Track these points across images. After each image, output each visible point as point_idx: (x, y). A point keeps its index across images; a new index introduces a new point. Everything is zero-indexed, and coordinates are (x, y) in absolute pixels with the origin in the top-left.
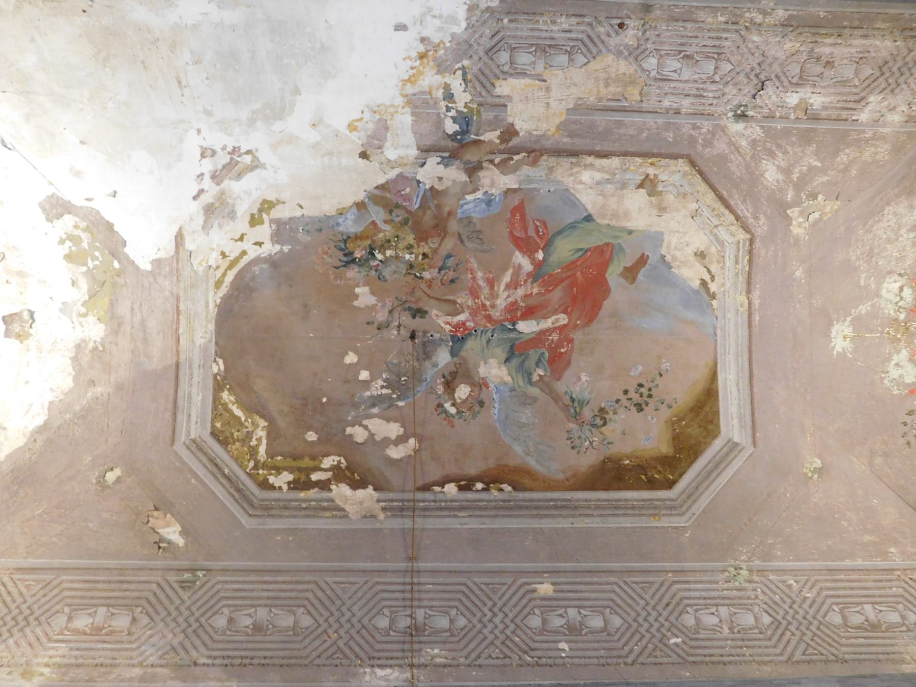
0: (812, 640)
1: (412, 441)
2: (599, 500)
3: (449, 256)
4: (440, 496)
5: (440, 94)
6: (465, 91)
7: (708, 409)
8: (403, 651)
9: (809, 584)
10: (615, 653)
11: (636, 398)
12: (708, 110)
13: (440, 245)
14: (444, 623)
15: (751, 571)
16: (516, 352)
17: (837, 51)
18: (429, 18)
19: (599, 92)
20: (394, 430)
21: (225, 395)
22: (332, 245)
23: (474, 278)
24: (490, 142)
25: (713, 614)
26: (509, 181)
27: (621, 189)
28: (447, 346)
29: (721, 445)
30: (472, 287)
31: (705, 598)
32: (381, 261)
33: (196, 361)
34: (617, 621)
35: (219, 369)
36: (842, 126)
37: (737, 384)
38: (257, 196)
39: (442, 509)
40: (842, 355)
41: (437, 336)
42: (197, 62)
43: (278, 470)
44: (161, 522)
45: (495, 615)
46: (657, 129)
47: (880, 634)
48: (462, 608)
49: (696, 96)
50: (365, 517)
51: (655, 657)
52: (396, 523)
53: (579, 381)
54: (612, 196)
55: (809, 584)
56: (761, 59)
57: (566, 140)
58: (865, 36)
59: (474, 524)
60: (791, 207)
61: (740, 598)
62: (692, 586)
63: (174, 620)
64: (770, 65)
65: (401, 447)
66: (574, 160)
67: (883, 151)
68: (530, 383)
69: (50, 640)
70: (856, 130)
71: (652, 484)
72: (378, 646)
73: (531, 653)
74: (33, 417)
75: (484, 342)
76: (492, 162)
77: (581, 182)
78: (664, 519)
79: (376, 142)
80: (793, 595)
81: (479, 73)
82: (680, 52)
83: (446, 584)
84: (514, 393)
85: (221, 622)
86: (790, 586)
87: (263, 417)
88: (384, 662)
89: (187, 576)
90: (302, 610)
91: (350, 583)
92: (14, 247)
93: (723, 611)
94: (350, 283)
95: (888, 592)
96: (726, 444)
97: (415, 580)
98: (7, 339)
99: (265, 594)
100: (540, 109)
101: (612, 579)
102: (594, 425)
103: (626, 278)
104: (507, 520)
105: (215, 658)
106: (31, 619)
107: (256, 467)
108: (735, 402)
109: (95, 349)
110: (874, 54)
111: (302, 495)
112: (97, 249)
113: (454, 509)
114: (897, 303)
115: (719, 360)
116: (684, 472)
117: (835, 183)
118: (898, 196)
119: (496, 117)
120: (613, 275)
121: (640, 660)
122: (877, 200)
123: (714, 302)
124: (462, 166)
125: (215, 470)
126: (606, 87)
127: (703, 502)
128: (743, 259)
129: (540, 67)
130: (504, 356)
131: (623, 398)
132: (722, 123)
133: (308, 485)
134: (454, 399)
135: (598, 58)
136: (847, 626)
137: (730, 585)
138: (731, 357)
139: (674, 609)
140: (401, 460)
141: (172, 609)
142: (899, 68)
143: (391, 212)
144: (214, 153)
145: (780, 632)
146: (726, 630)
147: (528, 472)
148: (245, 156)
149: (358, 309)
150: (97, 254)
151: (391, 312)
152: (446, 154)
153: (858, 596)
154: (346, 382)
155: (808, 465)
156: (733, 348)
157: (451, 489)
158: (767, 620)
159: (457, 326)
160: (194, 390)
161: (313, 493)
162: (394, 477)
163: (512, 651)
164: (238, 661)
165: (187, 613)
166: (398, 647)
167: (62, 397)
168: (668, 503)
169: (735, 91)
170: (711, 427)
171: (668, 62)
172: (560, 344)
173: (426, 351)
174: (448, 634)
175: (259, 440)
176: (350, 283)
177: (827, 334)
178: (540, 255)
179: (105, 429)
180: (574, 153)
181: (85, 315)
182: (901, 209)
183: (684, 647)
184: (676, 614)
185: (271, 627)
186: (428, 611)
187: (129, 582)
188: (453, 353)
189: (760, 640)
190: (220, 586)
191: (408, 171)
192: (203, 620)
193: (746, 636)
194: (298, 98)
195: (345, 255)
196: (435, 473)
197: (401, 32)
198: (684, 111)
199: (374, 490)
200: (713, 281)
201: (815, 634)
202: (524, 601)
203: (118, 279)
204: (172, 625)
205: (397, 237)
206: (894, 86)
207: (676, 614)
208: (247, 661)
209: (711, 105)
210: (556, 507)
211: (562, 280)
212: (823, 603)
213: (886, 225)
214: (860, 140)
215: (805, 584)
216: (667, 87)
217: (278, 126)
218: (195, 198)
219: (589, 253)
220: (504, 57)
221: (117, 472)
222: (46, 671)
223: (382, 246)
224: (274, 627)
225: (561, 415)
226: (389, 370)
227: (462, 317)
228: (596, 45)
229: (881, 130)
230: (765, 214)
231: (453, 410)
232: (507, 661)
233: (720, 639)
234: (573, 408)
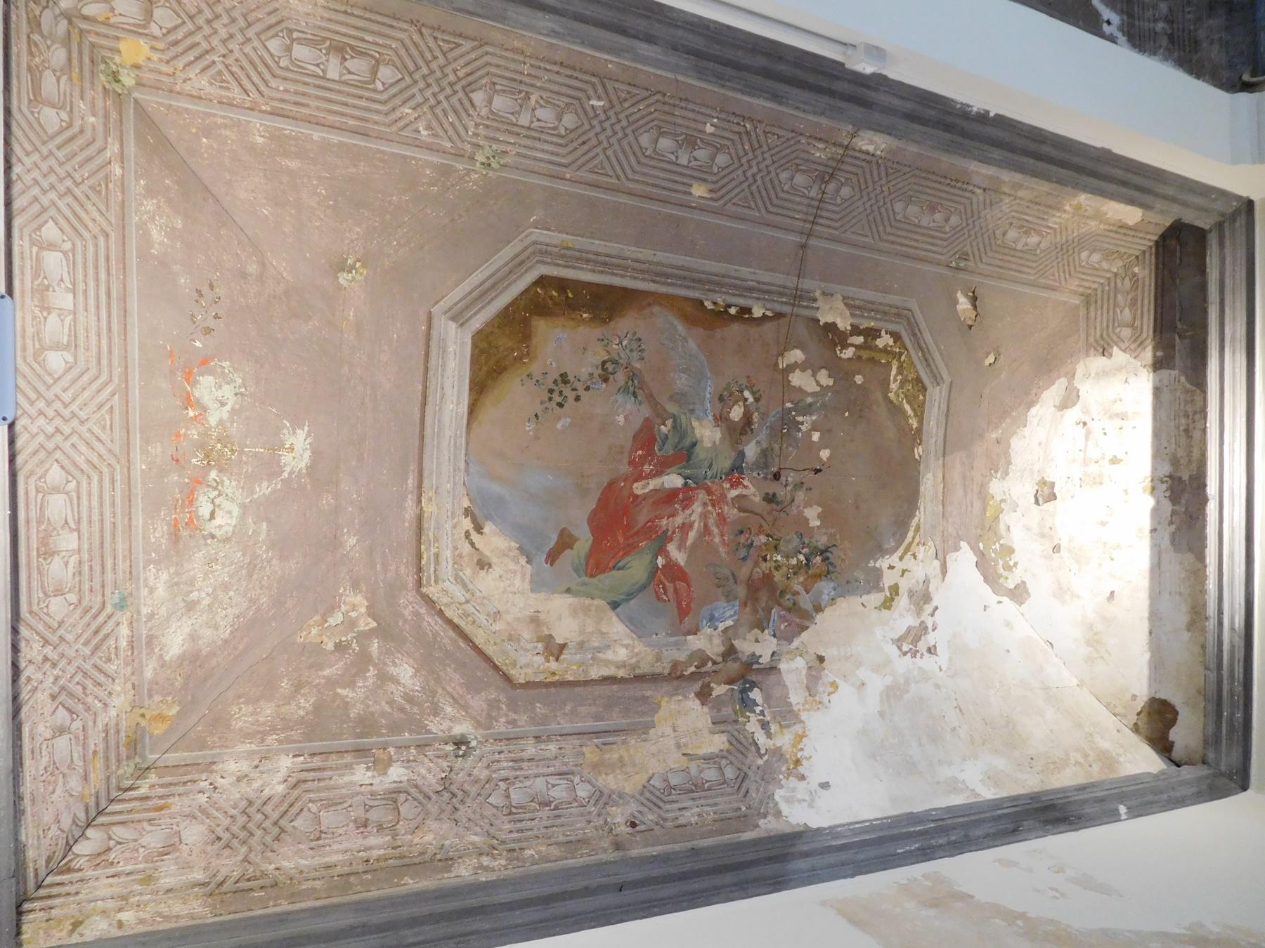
0: (435, 58)
2: (622, 276)
3: (744, 559)
4: (768, 306)
5: (774, 727)
7: (485, 368)
9: (402, 123)
10: (667, 108)
11: (567, 391)
12: (502, 746)
14: (800, 179)
15: (472, 158)
16: (685, 454)
17: (359, 842)
19: (628, 751)
20: (797, 379)
21: (914, 423)
23: (722, 535)
24: (719, 684)
25: (539, 120)
26: (696, 642)
29: (473, 321)
36: (317, 745)
37: (443, 396)
40: (297, 423)
42: (954, 729)
43: (885, 351)
47: (337, 38)
49: (522, 760)
51: (629, 92)
52: (807, 284)
53: (625, 415)
56: (457, 816)
57: (649, 693)
59: (745, 272)
60: (371, 630)
61: (498, 130)
64: (442, 811)
65: (792, 360)
66: (638, 671)
67: (242, 717)
68: (675, 418)
69: (1055, 230)
70: (294, 742)
71: (562, 284)
72: (859, 171)
75: (714, 466)
76: (715, 663)
77: (626, 646)
78: (556, 242)
82: (556, 808)
85: (954, 220)
86: (429, 127)
87: (891, 402)
88: (864, 157)
95: (292, 87)
97: (809, 226)
99: (917, 237)
101: (631, 185)
102: (615, 362)
103: (571, 536)
107: (901, 354)
108: (449, 373)
109: (996, 472)
110: (302, 846)
113: (759, 290)
116: (522, 294)
117: (311, 667)
118: (212, 654)
119: (719, 710)
120: (585, 539)
121: (646, 94)
122: (241, 647)
123: (466, 503)
124: (740, 655)
125: (928, 356)
126: (621, 757)
127: (507, 253)
129: (694, 770)
130: (697, 449)
131: (581, 392)
132: (481, 731)
135: (640, 787)
136: (377, 61)
137: (503, 148)
138: (448, 433)
146: (533, 98)
149: (819, 505)
152: (755, 666)
154: (829, 431)
155: (358, 277)
157: (758, 312)
158: (478, 97)
161: (865, 324)
162: (801, 331)
164: (959, 185)
169: (475, 772)
171: (564, 794)
172: (643, 459)
175: (895, 380)
177: (316, 454)
178: (660, 561)
180: (639, 678)
181: (1002, 501)
182: (207, 633)
184: (580, 131)
188: (741, 455)
191: (785, 647)
193: (514, 85)
196: (769, 327)
200: (467, 532)
202: (722, 183)
206: (251, 810)
209: (500, 753)
210: (667, 276)
211: (637, 533)
216: (557, 766)
217: (889, 680)
218: (936, 608)
220: (730, 773)
222: (1067, 208)
227: (734, 493)
230: (405, 621)
231: (747, 394)
234: (635, 386)
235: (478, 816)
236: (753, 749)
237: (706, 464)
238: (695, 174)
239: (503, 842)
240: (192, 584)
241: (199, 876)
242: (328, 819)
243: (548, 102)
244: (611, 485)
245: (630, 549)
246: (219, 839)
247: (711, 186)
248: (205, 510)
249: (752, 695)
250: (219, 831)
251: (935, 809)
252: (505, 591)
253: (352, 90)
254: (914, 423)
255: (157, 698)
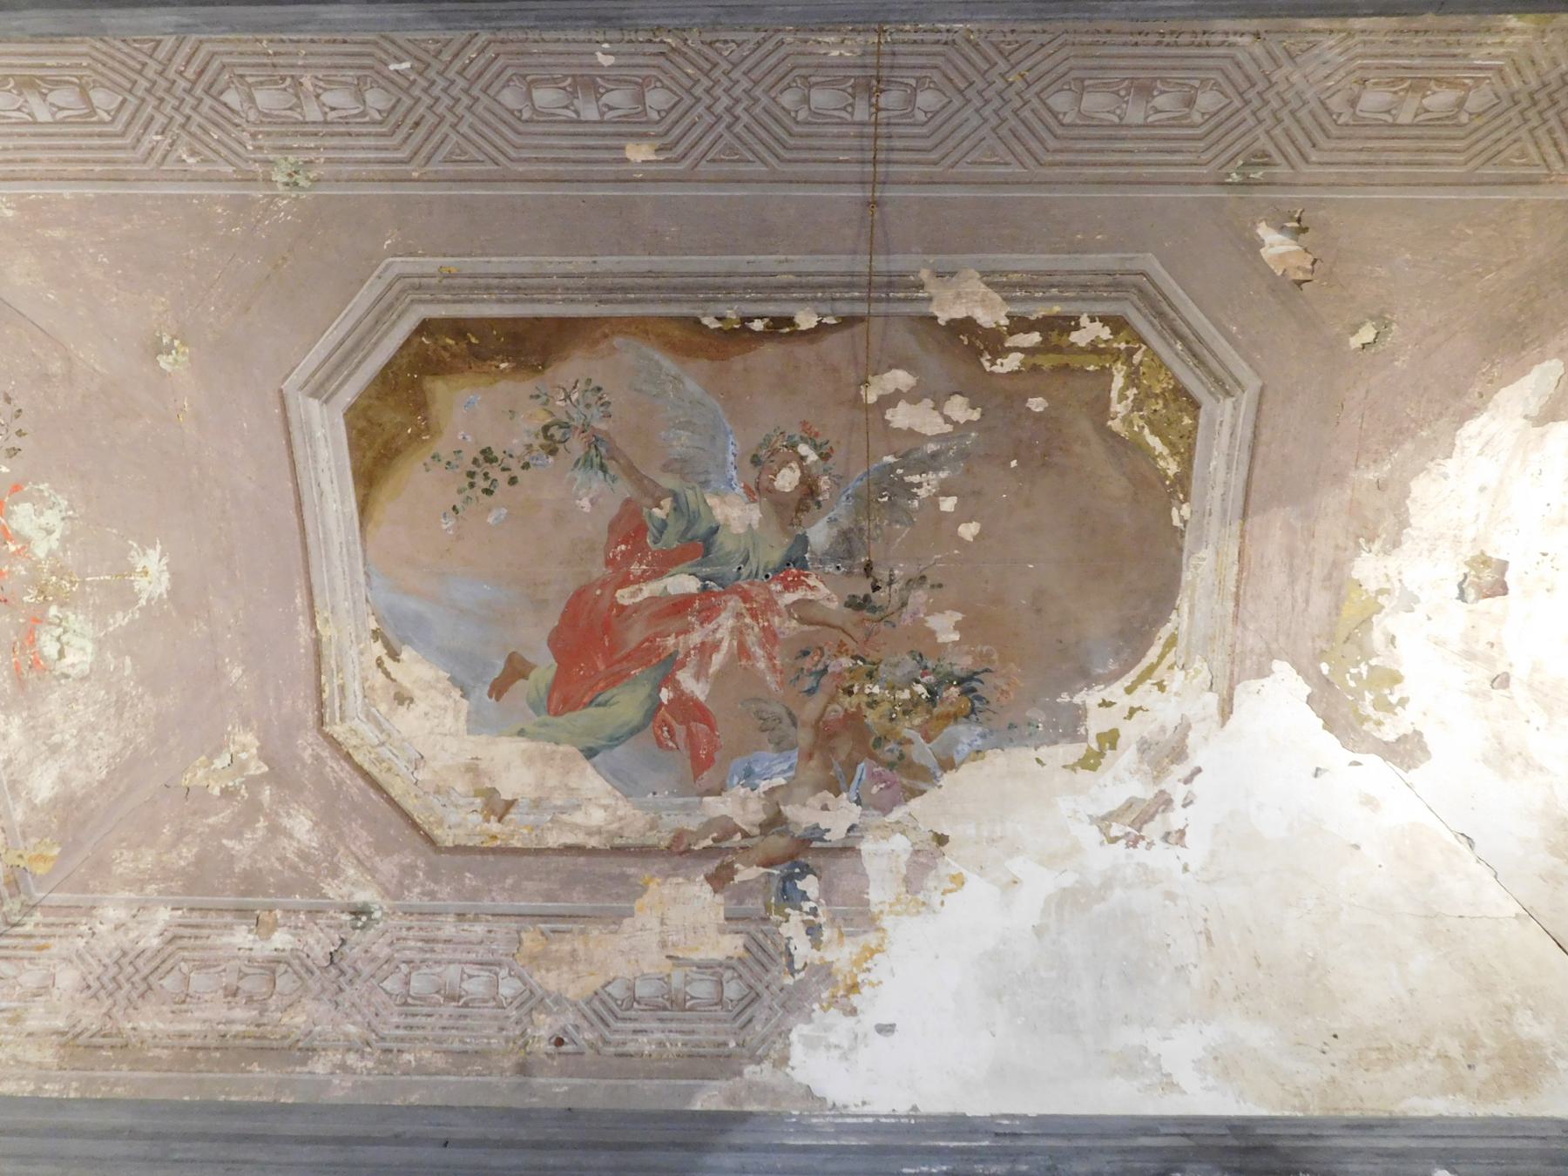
0: (144, 65)
1: (872, 398)
2: (549, 302)
3: (811, 691)
4: (825, 309)
5: (827, 933)
6: (789, 938)
7: (370, 454)
8: (894, 54)
9: (158, 155)
11: (495, 472)
13: (825, 707)
14: (820, 98)
15: (268, 180)
16: (700, 545)
17: (224, 1013)
18: (846, 1044)
19: (586, 944)
20: (900, 417)
21: (1172, 467)
22: (993, 706)
23: (771, 658)
24: (748, 865)
25: (333, 109)
26: (717, 807)
27: (540, 799)
28: (812, 553)
29: (341, 392)
30: (773, 646)
31: (350, 134)
32: (918, 682)
33: (1215, 521)
34: (509, 98)
35: (1179, 509)
36: (197, 900)
37: (321, 495)
38: (1105, 775)
39: (822, 287)
40: (146, 544)
41: (830, 568)
42: (1180, 969)
43: (1094, 349)
44: (1293, 261)
45: (728, 110)
46: (490, 891)
48: (787, 121)
49: (435, 941)
50: (952, 274)
52: (899, 262)
53: (592, 500)
54: (554, 788)
55: (158, 155)
56: (340, 998)
57: (632, 871)
58: (183, 1036)
59: (767, 261)
60: (263, 776)
61: (286, 135)
62: (372, 155)
63: (1285, 103)
64: (324, 990)
65: (890, 388)
66: (618, 842)
68: (675, 496)
69: (1500, 70)
70: (173, 894)
71: (458, 328)
73: (664, 49)
74: (1480, 434)
76: (746, 835)
79: (923, 860)
80: (186, 138)
81: (769, 966)
82: (466, 1005)
83: (815, 161)
84: (702, 478)
85: (1207, 100)
86: (193, 153)
87: (1115, 435)
89: (1258, 174)
90: (1067, 120)
91: (981, 163)
92: (1476, 696)
93: (313, 113)
94: (966, 648)
96: (333, 394)
97: (869, 168)
98: (1503, 557)
100: (675, 915)
102: (564, 426)
103: (524, 662)
104: (711, 268)
105: (1222, 44)
106: (1525, 103)
107: (1131, 353)
108: (322, 465)
109: (1370, 540)
110: (165, 1008)
111: (1057, 309)
112: (1351, 691)
113: (802, 287)
114: (65, 632)
115: (357, 533)
116: (402, 348)
117: (195, 813)
119: (741, 902)
120: (545, 667)
122: (122, 788)
123: (374, 625)
124: (791, 828)
125: (1197, 347)
127: (365, 296)
128: (332, 694)
129: (677, 979)
130: (720, 537)
131: (517, 471)
133: (1046, 325)
134: (802, 468)
135: (590, 993)
136: (80, 86)
138: (337, 538)
139: (405, 116)
140: (890, 368)
141: (1288, 121)
142: (120, 987)
143: (902, 756)
144: (1166, 837)
145: (206, 78)
146: (307, 82)
147: (673, 347)
148: (1119, 834)
149: (956, 608)
150: (1352, 684)
151: (904, 604)
153: (63, 135)
154: (977, 493)
155: (181, 358)
156: (335, 550)
158: (232, 98)
159: (797, 583)
160: (1221, 476)
161: (1038, 311)
162: (902, 338)
163: (699, 53)
164: (1182, 39)
165: (1263, 114)
166: (901, 60)
167: (1431, 465)
168: (428, 297)
169: (374, 948)
170: (362, 424)
171: (481, 989)
172: (628, 557)
173: (847, 545)
174: (813, 79)
175: (1122, 397)
176: (966, 648)
177: (175, 576)
178: (665, 695)
179: (1367, 413)
180: (619, 851)
181: (1381, 592)
183: (384, 56)
184: (401, 109)
185: (1123, 93)
186: (848, 117)
187: (1357, 164)
188: (803, 541)
189: (241, 65)
190: (1204, 157)
191: (875, 818)
192: (1237, 103)
194: (1036, 922)
195: (973, 690)
196: (834, 346)
197: (885, 1022)
198: (451, 919)
199: (936, 318)
201: (140, 73)
202: (677, 131)
203: (1325, 646)
204: (1288, 96)
205: (892, 720)
207: (401, 109)
208: (1167, 39)
209: (409, 929)
210: (625, 289)
211: (627, 657)
212: (129, 124)
213: (101, 751)
214: (164, 880)
215: (165, 157)
216: (481, 953)
217: (1069, 880)
218: (1199, 770)
219: (586, 700)
220: (732, 990)
221: (1355, 342)
223: (916, 705)
224: (1117, 93)
225: (620, 442)
226: (908, 512)
227: (790, 597)
228: (595, 1011)
229: (133, 895)
230: (304, 765)
231: (803, 449)
232: (708, 37)
233: (316, 67)
234: (601, 455)
235: (364, 1002)
236: (784, 960)
237: (738, 558)
238: (624, 129)
239: (383, 1039)
240: (51, 727)
241: (60, 1023)
242: (199, 981)
243: (330, 82)
244: (579, 594)
245: (616, 679)
246: (89, 987)
247: (658, 143)
248: (51, 649)
249: (800, 885)
250: (91, 979)
251: (1012, 1117)
252: (431, 733)
253: (76, 129)
254: (1172, 467)
255: (34, 840)
